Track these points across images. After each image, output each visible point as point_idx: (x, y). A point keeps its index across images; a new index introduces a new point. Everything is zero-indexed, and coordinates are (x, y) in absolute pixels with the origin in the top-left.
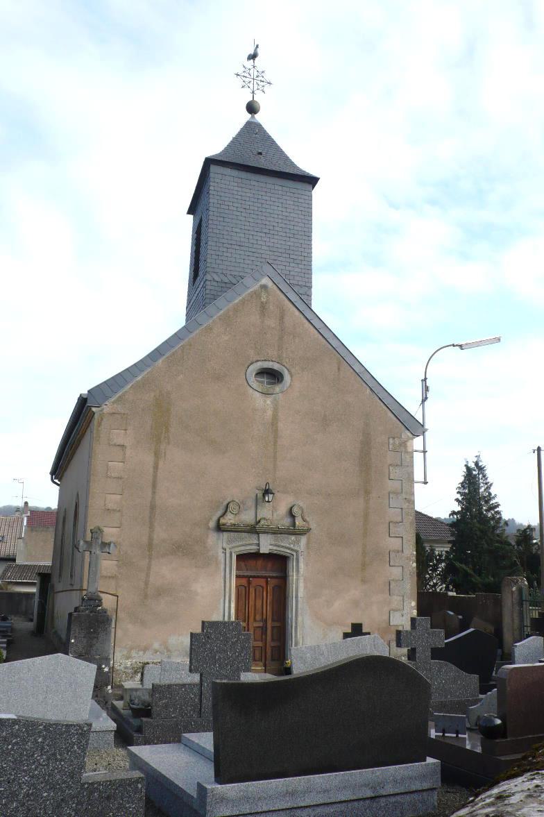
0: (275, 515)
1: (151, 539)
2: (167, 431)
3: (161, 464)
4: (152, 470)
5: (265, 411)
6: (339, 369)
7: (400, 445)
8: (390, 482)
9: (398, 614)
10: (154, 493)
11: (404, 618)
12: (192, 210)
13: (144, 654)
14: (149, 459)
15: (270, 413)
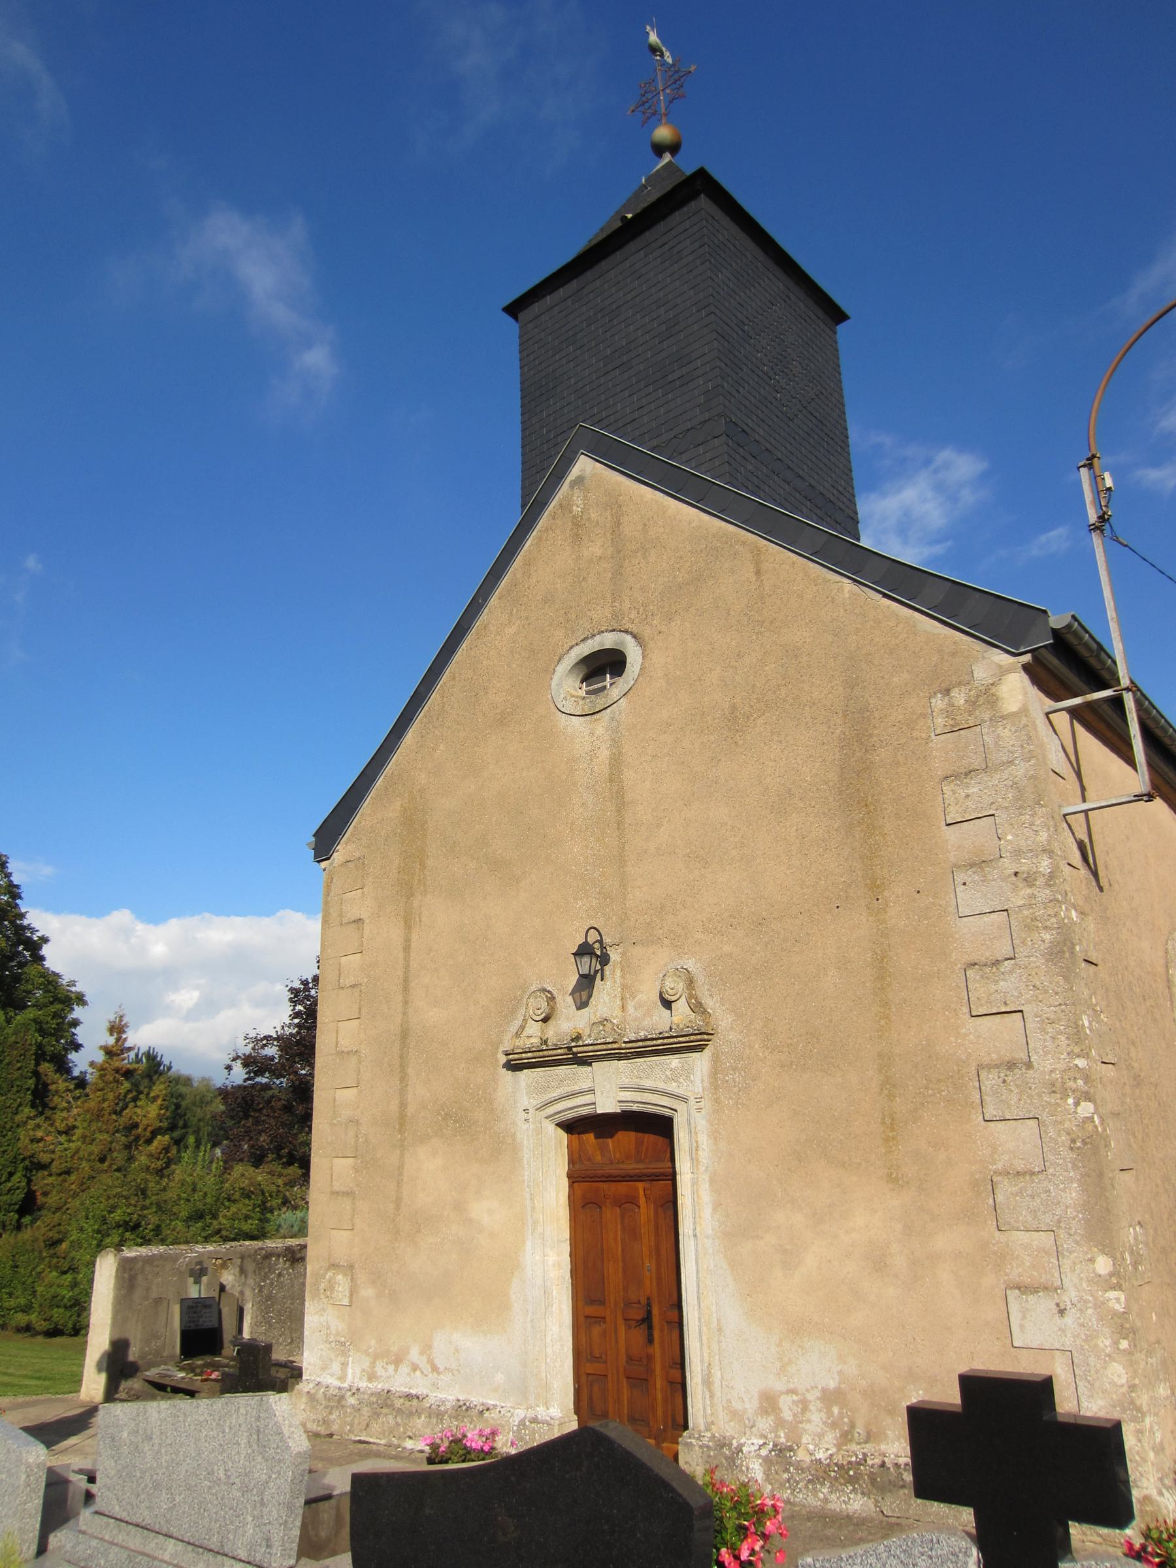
0: (630, 1009)
1: (403, 1105)
2: (423, 866)
3: (414, 937)
4: (401, 955)
5: (593, 756)
6: (758, 573)
7: (973, 703)
8: (951, 834)
9: (1042, 1305)
10: (406, 1003)
11: (1068, 1320)
12: (590, 1064)
13: (396, 1371)
14: (395, 933)
15: (604, 754)
